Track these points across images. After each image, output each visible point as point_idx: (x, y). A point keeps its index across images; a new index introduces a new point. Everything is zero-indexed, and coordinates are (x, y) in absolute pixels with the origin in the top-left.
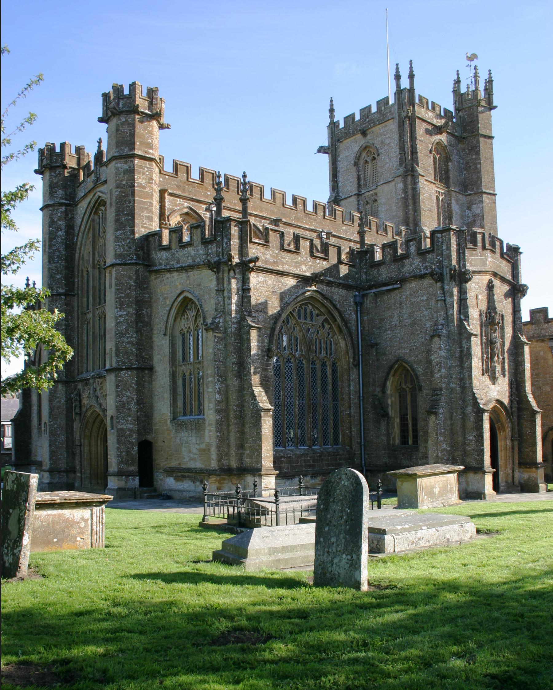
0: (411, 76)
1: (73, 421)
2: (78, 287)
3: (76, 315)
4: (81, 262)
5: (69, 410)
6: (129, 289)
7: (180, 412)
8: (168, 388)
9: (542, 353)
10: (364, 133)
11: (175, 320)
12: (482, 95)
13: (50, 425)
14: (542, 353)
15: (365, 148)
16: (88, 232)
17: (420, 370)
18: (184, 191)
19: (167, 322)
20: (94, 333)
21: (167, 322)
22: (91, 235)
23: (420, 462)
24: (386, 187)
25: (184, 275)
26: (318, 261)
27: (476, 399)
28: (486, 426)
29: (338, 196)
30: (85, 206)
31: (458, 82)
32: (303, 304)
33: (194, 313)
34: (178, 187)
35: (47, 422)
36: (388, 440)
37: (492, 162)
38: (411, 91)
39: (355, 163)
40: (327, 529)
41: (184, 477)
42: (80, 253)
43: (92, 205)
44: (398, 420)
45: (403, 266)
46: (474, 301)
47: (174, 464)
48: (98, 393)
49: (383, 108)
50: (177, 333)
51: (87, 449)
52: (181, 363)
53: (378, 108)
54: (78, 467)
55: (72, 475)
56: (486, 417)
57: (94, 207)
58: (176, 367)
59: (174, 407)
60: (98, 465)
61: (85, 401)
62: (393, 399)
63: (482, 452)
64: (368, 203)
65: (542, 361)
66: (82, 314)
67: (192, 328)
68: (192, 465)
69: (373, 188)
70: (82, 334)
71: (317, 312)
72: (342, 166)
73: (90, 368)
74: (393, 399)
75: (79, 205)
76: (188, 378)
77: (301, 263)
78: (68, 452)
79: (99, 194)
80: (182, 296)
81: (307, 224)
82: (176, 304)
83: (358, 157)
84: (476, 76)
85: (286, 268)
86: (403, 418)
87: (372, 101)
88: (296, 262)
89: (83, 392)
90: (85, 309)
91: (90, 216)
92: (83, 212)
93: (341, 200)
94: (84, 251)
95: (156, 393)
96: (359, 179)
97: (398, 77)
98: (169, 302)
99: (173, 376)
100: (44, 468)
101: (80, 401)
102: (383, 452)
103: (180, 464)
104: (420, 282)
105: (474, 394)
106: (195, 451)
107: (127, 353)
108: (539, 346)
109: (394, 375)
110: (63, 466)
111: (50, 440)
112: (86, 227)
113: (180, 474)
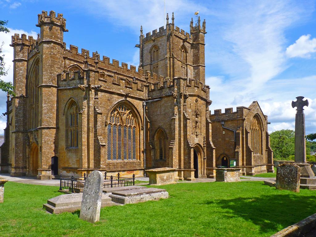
0: (173, 19)
1: (26, 148)
2: (29, 94)
3: (28, 106)
4: (31, 84)
5: (24, 144)
6: (49, 96)
7: (70, 145)
8: (64, 136)
9: (218, 126)
10: (154, 41)
11: (68, 109)
12: (201, 28)
13: (15, 150)
14: (218, 126)
15: (154, 46)
16: (34, 72)
17: (167, 131)
18: (75, 58)
19: (65, 109)
20: (35, 113)
21: (65, 109)
22: (35, 73)
23: (166, 166)
24: (162, 62)
25: (71, 91)
26: (128, 89)
27: (188, 143)
28: (192, 153)
29: (143, 64)
30: (32, 61)
31: (192, 23)
32: (121, 105)
33: (76, 107)
34: (72, 56)
35: (14, 148)
36: (155, 158)
37: (204, 54)
38: (173, 24)
39: (150, 51)
40: (86, 196)
41: (70, 171)
42: (30, 80)
43: (35, 61)
44: (159, 150)
45: (162, 92)
46: (189, 106)
47: (66, 166)
48: (36, 137)
49: (161, 31)
50: (69, 114)
51: (31, 160)
52: (70, 126)
53: (160, 31)
54: (27, 167)
55: (25, 170)
56: (192, 150)
57: (36, 62)
58: (68, 128)
59: (67, 143)
60: (36, 166)
61: (31, 140)
62: (157, 142)
63: (190, 163)
64: (154, 68)
65: (218, 129)
66: (31, 105)
67: (75, 112)
68: (73, 166)
69: (156, 62)
70: (31, 113)
71: (127, 108)
72: (145, 52)
73: (34, 127)
74: (157, 142)
75: (30, 61)
76: (73, 132)
77: (120, 89)
78: (23, 160)
79: (38, 56)
80: (70, 100)
81: (128, 74)
82: (68, 103)
83: (151, 49)
84: (199, 21)
85: (114, 91)
86: (161, 150)
87: (157, 28)
88: (118, 89)
89: (30, 137)
90: (32, 103)
91: (34, 66)
92: (31, 63)
93: (144, 66)
94: (32, 79)
95: (60, 138)
96: (151, 58)
97: (168, 19)
98: (65, 102)
99: (67, 131)
100: (12, 167)
101: (29, 140)
102: (153, 162)
103: (68, 166)
104: (168, 98)
105: (188, 141)
106: (75, 161)
107: (47, 121)
108: (218, 125)
109: (157, 133)
110: (21, 165)
111: (15, 156)
112: (33, 70)
113: (68, 170)
